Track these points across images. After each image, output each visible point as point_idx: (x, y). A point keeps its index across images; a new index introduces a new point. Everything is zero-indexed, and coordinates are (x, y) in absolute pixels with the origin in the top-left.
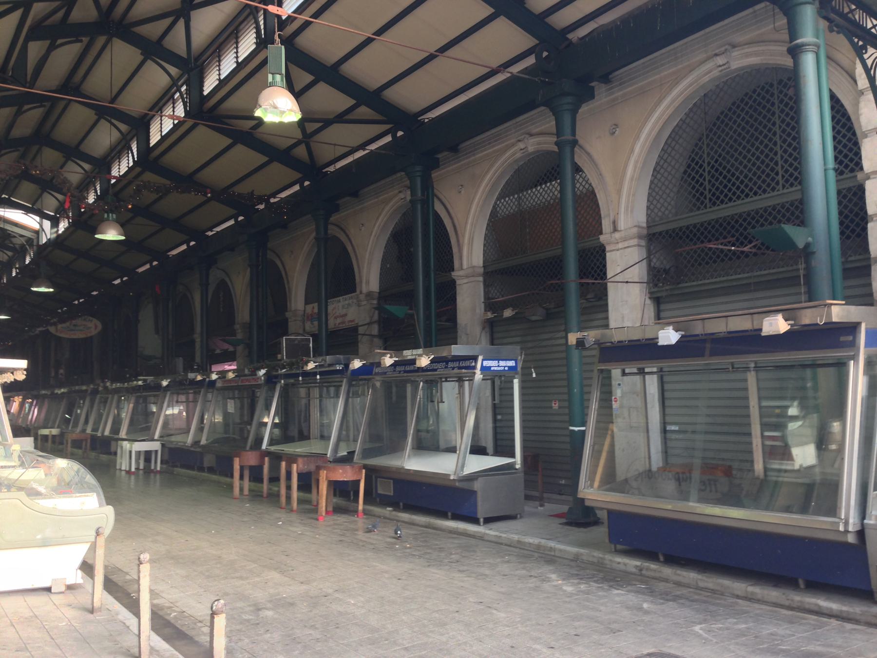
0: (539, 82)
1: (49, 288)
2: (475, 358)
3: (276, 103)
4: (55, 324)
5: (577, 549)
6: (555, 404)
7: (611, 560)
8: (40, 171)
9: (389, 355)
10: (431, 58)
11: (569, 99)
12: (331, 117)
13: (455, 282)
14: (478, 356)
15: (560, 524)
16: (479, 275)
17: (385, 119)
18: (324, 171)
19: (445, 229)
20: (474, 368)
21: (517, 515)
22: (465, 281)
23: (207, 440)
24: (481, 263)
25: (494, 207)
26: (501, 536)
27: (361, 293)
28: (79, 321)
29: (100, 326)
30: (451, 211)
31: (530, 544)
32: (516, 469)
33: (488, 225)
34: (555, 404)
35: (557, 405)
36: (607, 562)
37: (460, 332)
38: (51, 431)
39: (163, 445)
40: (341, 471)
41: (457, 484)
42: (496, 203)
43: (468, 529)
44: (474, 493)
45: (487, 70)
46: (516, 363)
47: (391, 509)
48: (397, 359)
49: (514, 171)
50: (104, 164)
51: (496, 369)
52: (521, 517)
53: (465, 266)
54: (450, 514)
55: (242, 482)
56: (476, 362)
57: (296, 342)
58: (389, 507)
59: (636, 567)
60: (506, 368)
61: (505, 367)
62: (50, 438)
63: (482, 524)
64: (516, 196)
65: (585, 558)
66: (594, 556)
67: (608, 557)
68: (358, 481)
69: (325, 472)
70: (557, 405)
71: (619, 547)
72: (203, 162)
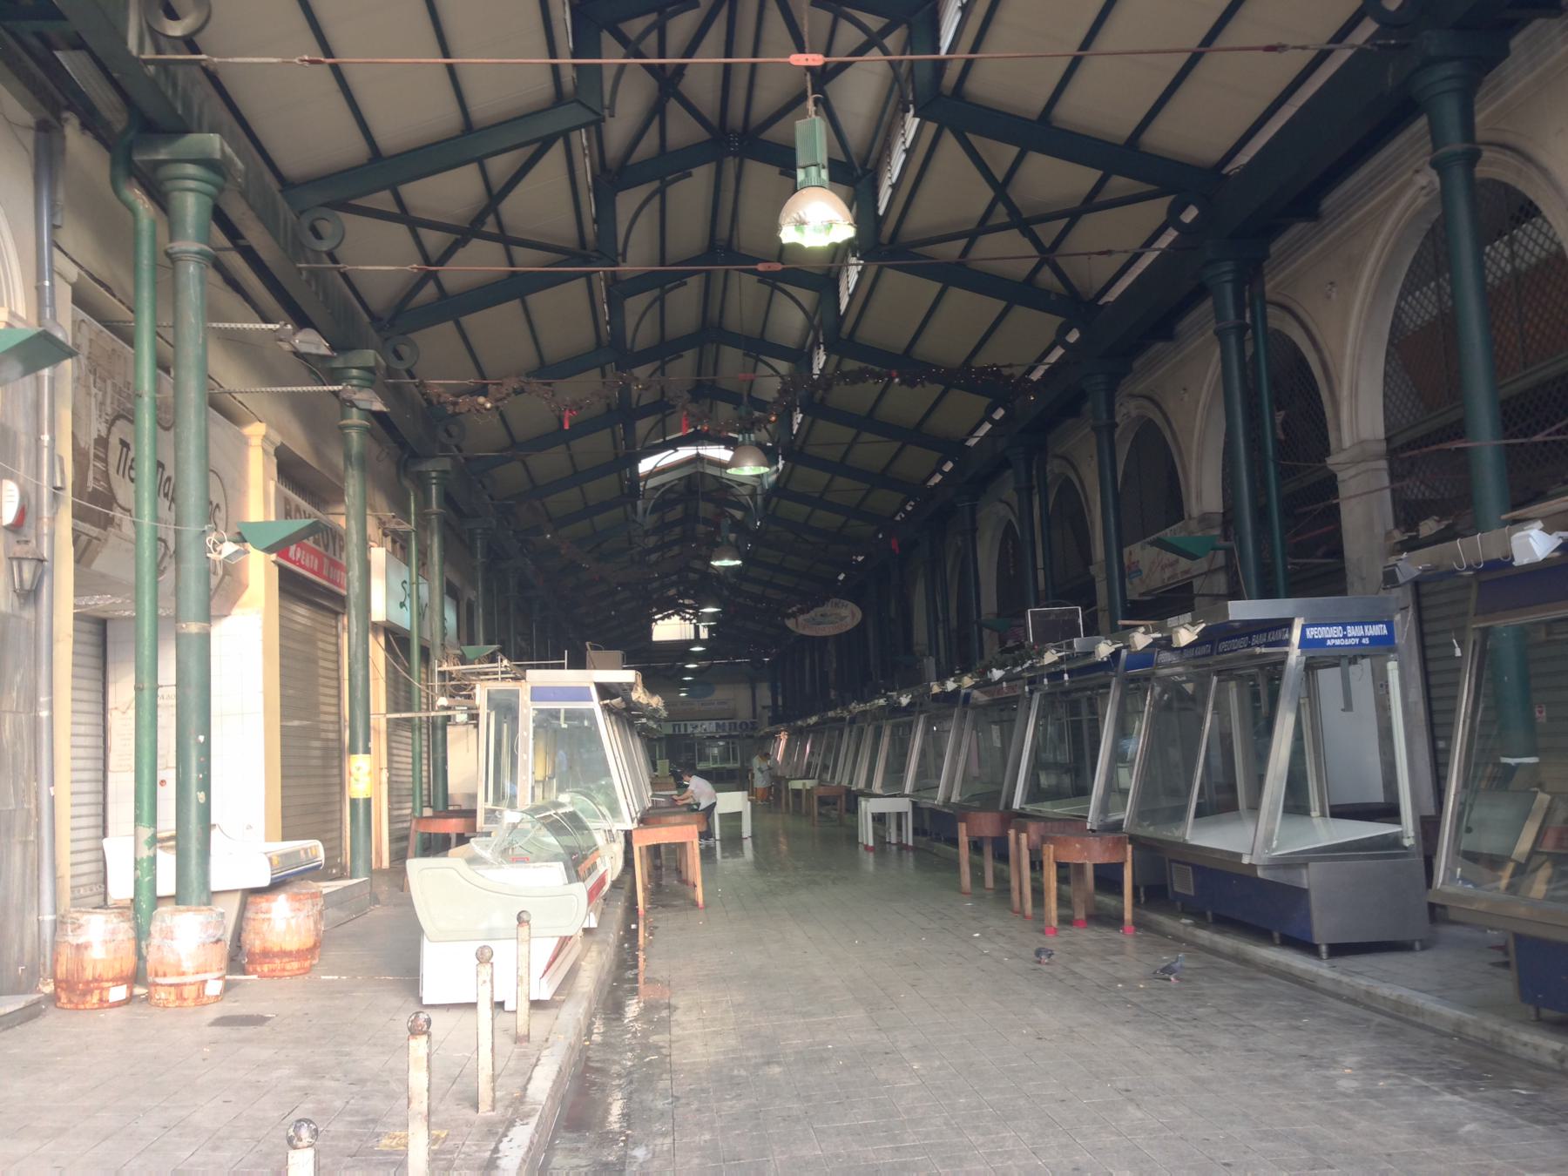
0: (1376, 49)
1: (734, 559)
2: (1287, 624)
3: (803, 215)
4: (794, 615)
5: (1458, 1013)
6: (1541, 712)
7: (1511, 1038)
8: (643, 384)
9: (1142, 629)
10: (1076, 62)
11: (1448, 69)
12: (1077, 203)
13: (1336, 476)
14: (1293, 619)
15: (1494, 964)
16: (1377, 457)
17: (1156, 188)
18: (1101, 303)
19: (1313, 377)
20: (1287, 643)
21: (1414, 941)
22: (1352, 472)
23: (960, 795)
24: (1380, 432)
25: (1396, 316)
26: (1340, 982)
27: (1190, 517)
28: (827, 608)
29: (859, 615)
30: (1319, 338)
31: (1384, 998)
32: (1406, 848)
33: (1388, 353)
34: (1541, 712)
35: (1544, 714)
36: (1506, 1041)
37: (1351, 577)
38: (804, 784)
39: (914, 804)
40: (1077, 846)
41: (1260, 874)
42: (1398, 307)
43: (1293, 964)
44: (1301, 894)
45: (1186, 57)
46: (1390, 629)
47: (1188, 921)
48: (1159, 635)
49: (1424, 234)
50: (801, 357)
51: (1338, 642)
52: (1423, 948)
53: (1347, 443)
54: (1276, 935)
55: (1037, 875)
56: (1290, 632)
57: (1052, 617)
58: (1186, 918)
59: (1554, 1053)
60: (1365, 641)
61: (1361, 638)
62: (804, 793)
63: (1324, 956)
64: (1433, 284)
65: (1471, 1031)
66: (1484, 1029)
67: (1509, 1031)
68: (1120, 866)
69: (1052, 846)
70: (1544, 714)
71: (1546, 1013)
72: (920, 321)
